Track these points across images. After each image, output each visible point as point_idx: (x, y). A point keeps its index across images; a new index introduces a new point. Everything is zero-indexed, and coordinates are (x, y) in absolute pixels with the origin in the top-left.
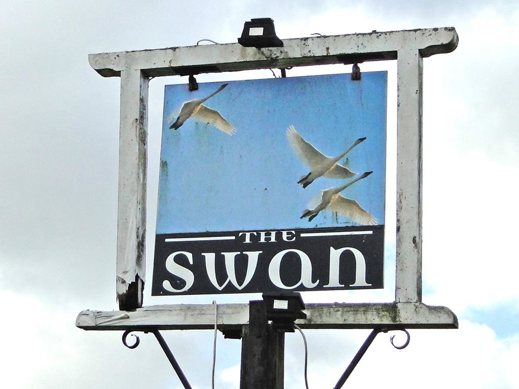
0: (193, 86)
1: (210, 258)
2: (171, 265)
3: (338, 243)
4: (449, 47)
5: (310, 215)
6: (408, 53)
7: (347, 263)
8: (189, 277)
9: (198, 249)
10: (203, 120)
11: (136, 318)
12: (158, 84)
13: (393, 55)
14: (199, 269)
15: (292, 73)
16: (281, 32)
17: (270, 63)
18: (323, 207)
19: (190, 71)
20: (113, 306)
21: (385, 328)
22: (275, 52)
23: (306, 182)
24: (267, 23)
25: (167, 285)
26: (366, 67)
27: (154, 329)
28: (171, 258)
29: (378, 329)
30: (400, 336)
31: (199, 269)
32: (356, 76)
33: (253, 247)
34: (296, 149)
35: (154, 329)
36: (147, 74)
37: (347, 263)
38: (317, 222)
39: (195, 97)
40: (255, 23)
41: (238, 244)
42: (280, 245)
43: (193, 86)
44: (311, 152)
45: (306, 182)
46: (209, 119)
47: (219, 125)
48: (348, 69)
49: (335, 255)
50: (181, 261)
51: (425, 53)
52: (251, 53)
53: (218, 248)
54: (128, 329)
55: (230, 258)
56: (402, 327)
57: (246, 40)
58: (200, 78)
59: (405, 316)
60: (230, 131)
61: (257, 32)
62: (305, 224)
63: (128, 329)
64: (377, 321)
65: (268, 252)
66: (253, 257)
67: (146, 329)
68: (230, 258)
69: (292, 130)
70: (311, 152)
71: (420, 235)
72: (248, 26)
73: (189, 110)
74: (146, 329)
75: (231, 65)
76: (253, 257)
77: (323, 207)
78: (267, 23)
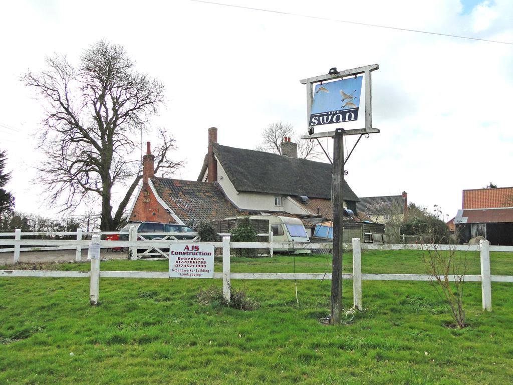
0: (321, 84)
1: (321, 118)
2: (313, 120)
3: (348, 112)
4: (377, 68)
5: (343, 107)
6: (367, 71)
7: (350, 116)
8: (316, 122)
9: (319, 116)
10: (322, 91)
11: (312, 136)
12: (314, 85)
13: (363, 72)
14: (319, 120)
15: (343, 78)
16: (338, 70)
17: (338, 77)
18: (346, 105)
19: (321, 81)
20: (308, 134)
21: (364, 134)
22: (338, 75)
23: (343, 101)
24: (335, 69)
25: (312, 124)
26: (358, 75)
27: (316, 138)
28: (313, 119)
29: (362, 134)
30: (367, 135)
31: (319, 120)
32: (356, 78)
33: (330, 115)
34: (341, 93)
35: (316, 138)
36: (312, 83)
37: (350, 116)
38: (344, 108)
39: (322, 86)
40: (332, 69)
41: (327, 114)
42: (336, 113)
43: (321, 84)
44: (345, 94)
45: (343, 101)
46: (324, 90)
47: (326, 91)
48: (354, 76)
49: (348, 114)
50: (315, 119)
51: (371, 71)
52: (333, 76)
53: (323, 116)
54: (311, 138)
55: (325, 117)
56: (367, 133)
57: (330, 73)
58: (323, 82)
59: (367, 131)
60: (328, 92)
61: (332, 71)
62: (342, 109)
63: (311, 138)
64: (362, 133)
65: (333, 115)
66: (330, 117)
67: (315, 138)
68: (325, 117)
69: (341, 90)
70: (345, 94)
71: (371, 113)
72: (330, 70)
73: (320, 89)
74: (315, 138)
75: (501, 253)
76: (330, 117)
77: (346, 105)
78: (335, 69)
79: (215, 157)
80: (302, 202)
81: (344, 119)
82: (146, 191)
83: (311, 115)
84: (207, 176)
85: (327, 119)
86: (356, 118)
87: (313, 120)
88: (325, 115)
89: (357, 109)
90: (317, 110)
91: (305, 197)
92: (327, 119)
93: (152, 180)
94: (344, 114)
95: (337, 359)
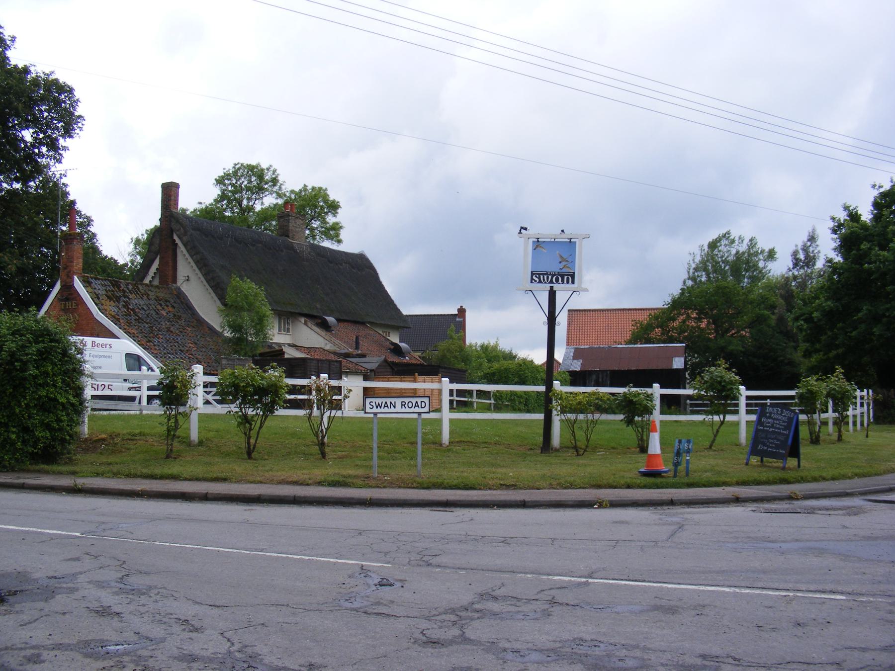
1: (542, 276)
2: (534, 277)
3: (566, 275)
5: (561, 269)
7: (568, 279)
8: (538, 280)
23: (560, 262)
31: (539, 278)
32: (570, 241)
37: (568, 279)
39: (539, 243)
42: (555, 275)
44: (561, 257)
49: (566, 277)
53: (543, 275)
55: (545, 277)
60: (545, 251)
66: (550, 277)
68: (545, 277)
70: (561, 257)
76: (550, 277)
79: (175, 237)
80: (324, 326)
81: (563, 281)
82: (67, 299)
83: (532, 272)
84: (157, 269)
85: (548, 278)
86: (573, 282)
87: (534, 277)
88: (545, 274)
89: (574, 273)
90: (541, 268)
91: (331, 319)
92: (548, 278)
93: (513, 382)
94: (562, 276)
95: (118, 659)
